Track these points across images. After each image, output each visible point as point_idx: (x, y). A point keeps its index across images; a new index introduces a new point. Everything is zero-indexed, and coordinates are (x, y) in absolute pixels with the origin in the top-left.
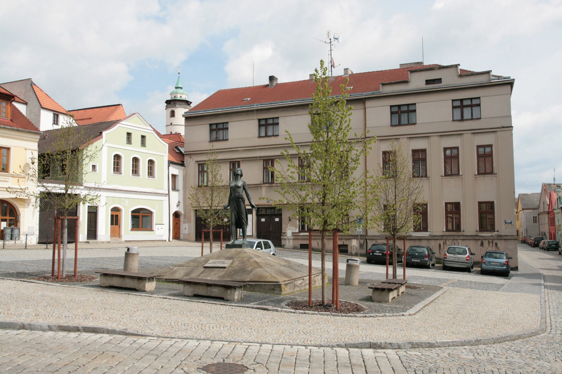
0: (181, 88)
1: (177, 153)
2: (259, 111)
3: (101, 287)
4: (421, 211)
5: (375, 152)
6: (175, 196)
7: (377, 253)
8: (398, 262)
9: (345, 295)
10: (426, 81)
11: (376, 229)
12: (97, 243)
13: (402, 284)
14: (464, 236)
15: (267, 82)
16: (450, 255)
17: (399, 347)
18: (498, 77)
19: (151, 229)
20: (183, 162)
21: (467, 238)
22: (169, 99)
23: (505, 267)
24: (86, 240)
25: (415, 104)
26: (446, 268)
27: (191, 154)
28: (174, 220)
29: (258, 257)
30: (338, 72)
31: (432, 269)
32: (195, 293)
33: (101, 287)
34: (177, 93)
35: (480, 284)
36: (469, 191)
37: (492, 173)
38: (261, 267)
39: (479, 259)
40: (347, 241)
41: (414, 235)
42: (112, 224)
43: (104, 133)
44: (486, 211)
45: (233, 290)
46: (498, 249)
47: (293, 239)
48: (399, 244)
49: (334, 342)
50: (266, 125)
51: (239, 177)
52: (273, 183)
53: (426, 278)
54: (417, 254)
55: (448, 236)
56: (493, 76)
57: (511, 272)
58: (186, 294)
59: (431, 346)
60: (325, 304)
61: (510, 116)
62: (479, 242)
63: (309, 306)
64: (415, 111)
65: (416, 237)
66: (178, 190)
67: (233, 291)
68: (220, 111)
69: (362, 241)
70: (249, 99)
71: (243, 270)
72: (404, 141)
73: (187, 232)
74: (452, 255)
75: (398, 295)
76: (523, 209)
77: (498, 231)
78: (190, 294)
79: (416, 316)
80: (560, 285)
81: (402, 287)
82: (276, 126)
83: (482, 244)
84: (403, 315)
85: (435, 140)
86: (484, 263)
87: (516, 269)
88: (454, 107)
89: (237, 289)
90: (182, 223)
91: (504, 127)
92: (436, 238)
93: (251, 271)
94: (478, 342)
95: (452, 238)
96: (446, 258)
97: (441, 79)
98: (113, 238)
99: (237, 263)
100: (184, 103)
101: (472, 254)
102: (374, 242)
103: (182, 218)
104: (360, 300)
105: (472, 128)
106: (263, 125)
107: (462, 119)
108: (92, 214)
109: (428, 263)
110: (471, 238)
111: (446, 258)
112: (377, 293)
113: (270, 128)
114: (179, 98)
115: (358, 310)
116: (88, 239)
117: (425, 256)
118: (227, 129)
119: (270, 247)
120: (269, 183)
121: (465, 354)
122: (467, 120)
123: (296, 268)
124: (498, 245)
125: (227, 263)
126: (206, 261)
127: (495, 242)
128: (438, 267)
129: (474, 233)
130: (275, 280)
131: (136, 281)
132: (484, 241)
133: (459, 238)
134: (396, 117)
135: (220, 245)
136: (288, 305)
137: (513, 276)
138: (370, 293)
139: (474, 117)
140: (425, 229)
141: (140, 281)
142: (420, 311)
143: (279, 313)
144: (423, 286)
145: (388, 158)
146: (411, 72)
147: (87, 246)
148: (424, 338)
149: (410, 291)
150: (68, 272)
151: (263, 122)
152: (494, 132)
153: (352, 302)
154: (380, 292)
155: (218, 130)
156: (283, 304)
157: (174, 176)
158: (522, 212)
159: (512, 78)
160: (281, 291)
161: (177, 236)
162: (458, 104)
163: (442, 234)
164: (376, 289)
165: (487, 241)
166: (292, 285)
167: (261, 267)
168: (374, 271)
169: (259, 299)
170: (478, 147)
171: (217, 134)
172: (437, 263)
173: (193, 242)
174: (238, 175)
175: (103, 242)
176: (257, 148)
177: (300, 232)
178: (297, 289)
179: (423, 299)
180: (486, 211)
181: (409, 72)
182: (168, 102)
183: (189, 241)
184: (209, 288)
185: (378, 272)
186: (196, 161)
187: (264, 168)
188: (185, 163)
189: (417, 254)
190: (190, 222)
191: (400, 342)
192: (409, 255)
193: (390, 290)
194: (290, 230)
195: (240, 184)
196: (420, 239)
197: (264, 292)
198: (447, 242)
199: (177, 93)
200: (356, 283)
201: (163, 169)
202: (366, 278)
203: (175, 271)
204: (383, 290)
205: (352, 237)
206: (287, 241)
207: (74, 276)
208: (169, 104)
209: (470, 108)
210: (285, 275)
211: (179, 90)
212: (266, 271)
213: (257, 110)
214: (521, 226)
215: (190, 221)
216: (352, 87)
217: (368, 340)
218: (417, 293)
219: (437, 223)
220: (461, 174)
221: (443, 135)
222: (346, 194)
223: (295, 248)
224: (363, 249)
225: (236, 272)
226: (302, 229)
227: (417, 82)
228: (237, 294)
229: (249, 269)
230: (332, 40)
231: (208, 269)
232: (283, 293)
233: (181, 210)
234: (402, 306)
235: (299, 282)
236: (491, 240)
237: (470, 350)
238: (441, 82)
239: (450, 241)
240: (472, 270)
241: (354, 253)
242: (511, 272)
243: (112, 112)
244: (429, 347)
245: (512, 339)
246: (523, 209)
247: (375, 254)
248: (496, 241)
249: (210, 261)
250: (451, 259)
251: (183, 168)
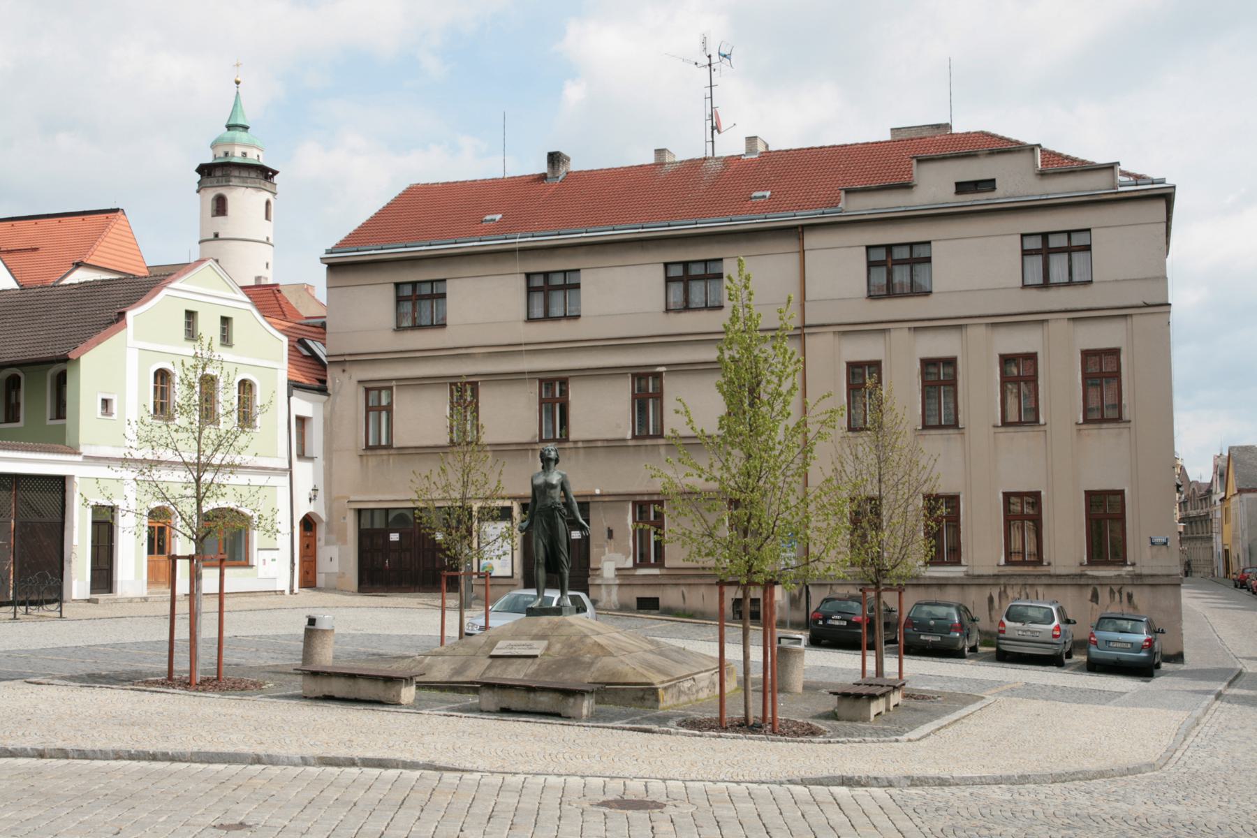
0: (246, 128)
1: (305, 357)
2: (526, 251)
4: (944, 516)
5: (828, 361)
6: (306, 475)
7: (836, 621)
8: (887, 643)
9: (786, 709)
10: (957, 184)
11: (833, 557)
12: (116, 601)
13: (895, 688)
14: (1050, 576)
15: (542, 167)
16: (1013, 624)
17: (890, 784)
18: (1137, 177)
19: (247, 565)
20: (324, 382)
21: (1057, 581)
22: (209, 159)
23: (1143, 654)
24: (88, 596)
25: (929, 243)
26: (1004, 657)
27: (344, 362)
28: (302, 537)
29: (598, 634)
30: (731, 145)
31: (970, 658)
32: (504, 705)
34: (232, 143)
35: (1073, 691)
36: (1064, 462)
37: (1119, 419)
38: (611, 655)
39: (1085, 636)
41: (927, 574)
42: (151, 552)
43: (131, 315)
44: (1105, 515)
45: (579, 698)
46: (1135, 608)
47: (620, 585)
48: (890, 599)
49: (783, 776)
50: (547, 289)
51: (552, 464)
52: (567, 440)
53: (950, 679)
54: (932, 622)
55: (1011, 576)
56: (1125, 174)
57: (1164, 665)
59: (942, 782)
60: (751, 722)
61: (1165, 278)
62: (1088, 593)
63: (721, 726)
64: (928, 260)
65: (931, 578)
66: (312, 459)
67: (579, 700)
68: (423, 249)
70: (498, 217)
71: (573, 661)
72: (900, 336)
73: (335, 567)
74: (1019, 625)
75: (888, 710)
76: (1240, 491)
77: (1133, 565)
78: (493, 708)
79: (921, 743)
80: (1252, 693)
81: (896, 693)
82: (573, 292)
83: (1095, 598)
84: (897, 741)
85: (977, 333)
86: (1095, 643)
87: (1178, 657)
88: (1025, 253)
89: (587, 696)
90: (320, 544)
91: (1148, 306)
92: (982, 581)
93: (592, 664)
94: (1024, 779)
95: (1020, 581)
96: (1003, 632)
97: (993, 180)
98: (154, 589)
99: (558, 646)
100: (253, 175)
101: (1068, 622)
102: (826, 593)
103: (321, 532)
104: (813, 717)
105: (1069, 307)
106: (538, 289)
107: (1046, 284)
108: (102, 527)
109: (960, 645)
110: (1068, 581)
111: (1003, 632)
112: (846, 702)
113: (557, 297)
114: (237, 158)
115: (813, 732)
116: (92, 593)
117: (953, 628)
118: (443, 296)
119: (585, 610)
120: (554, 440)
121: (998, 793)
122: (1058, 285)
123: (674, 655)
124: (1135, 598)
125: (538, 648)
126: (493, 645)
127: (1126, 590)
128: (986, 653)
129: (1075, 570)
130: (644, 680)
131: (380, 685)
132: (1099, 589)
133: (1037, 581)
134: (1036, 263)
135: (439, 602)
136: (679, 725)
137: (1166, 673)
138: (832, 703)
139: (1076, 278)
140: (955, 557)
141: (389, 684)
142: (929, 735)
143: (673, 737)
144: (940, 694)
145: (862, 376)
146: (920, 161)
147: (92, 610)
148: (932, 772)
149: (913, 703)
150: (204, 672)
151: (538, 282)
152: (1125, 316)
153: (800, 720)
154: (853, 700)
155: (419, 302)
156: (672, 723)
157: (301, 421)
158: (1237, 498)
159: (1169, 182)
160: (657, 700)
161: (310, 577)
162: (1035, 243)
163: (996, 571)
164: (844, 696)
165: (1108, 589)
166: (675, 690)
167: (611, 655)
168: (829, 664)
169: (626, 716)
170: (1086, 354)
171: (414, 310)
172: (984, 644)
173: (352, 593)
174: (550, 459)
175: (131, 600)
176: (523, 348)
177: (636, 566)
178: (684, 699)
179: (938, 717)
180: (1105, 515)
181: (914, 162)
182: (205, 171)
183: (343, 591)
184: (532, 695)
185: (843, 666)
186: (359, 382)
187: (542, 401)
188: (329, 384)
189: (932, 622)
190: (344, 542)
191: (892, 775)
192: (914, 625)
193: (872, 697)
194: (610, 562)
195: (555, 478)
196: (942, 584)
197: (629, 701)
198: (1009, 591)
199: (232, 143)
200: (799, 689)
201: (279, 406)
202: (814, 678)
203: (430, 667)
204: (858, 696)
206: (603, 590)
207: (218, 678)
208: (209, 175)
209: (1065, 256)
210: (660, 671)
211: (238, 134)
212: (622, 662)
213: (523, 250)
214: (1235, 538)
215: (342, 540)
216: (768, 194)
217: (838, 773)
218: (924, 705)
219: (984, 545)
220: (1042, 421)
221: (999, 322)
222: (789, 518)
223: (623, 608)
225: (561, 665)
226: (642, 561)
227: (935, 185)
228: (587, 706)
229: (588, 658)
230: (715, 58)
231: (500, 661)
232: (662, 705)
233: (318, 509)
234: (893, 726)
235: (686, 685)
236: (1116, 588)
237: (1009, 790)
238: (994, 189)
239: (1017, 589)
240: (1067, 661)
242: (1164, 665)
243: (99, 233)
244: (940, 785)
245: (1087, 776)
246: (1240, 491)
247: (830, 622)
248: (1129, 589)
249: (500, 644)
250: (1016, 635)
251: (324, 398)
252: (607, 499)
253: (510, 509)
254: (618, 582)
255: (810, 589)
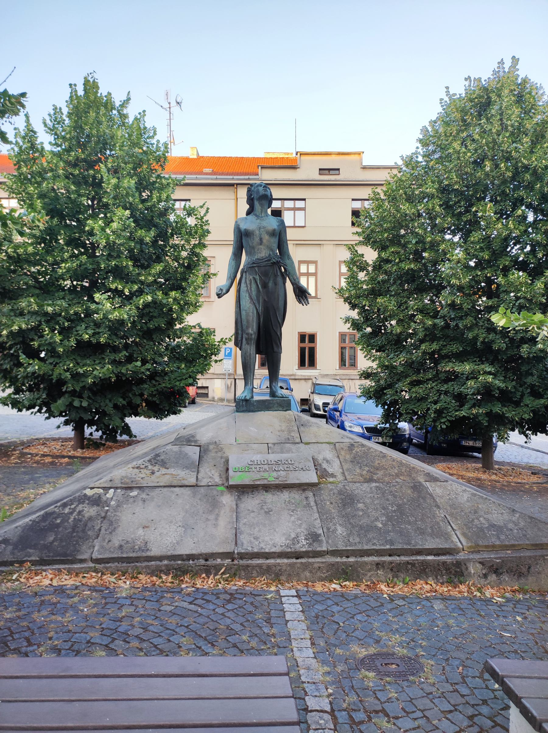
255: (237, 380)
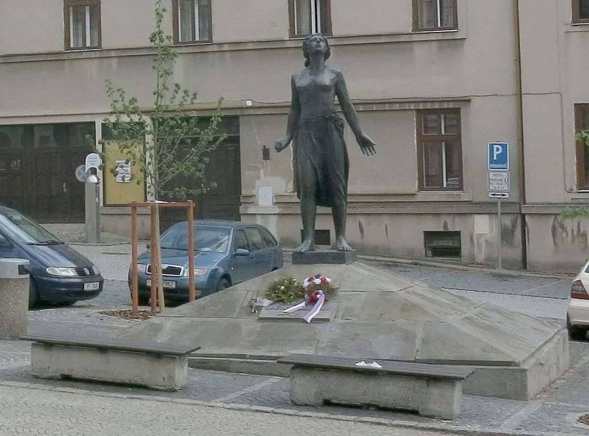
3: (36, 377)
33: (36, 378)
40: (458, 219)
58: (301, 397)
69: (507, 221)
163: (568, 198)
174: (318, 53)
195: (326, 79)
205: (475, 209)
224: (511, 244)
241: (481, 257)
252: (261, 112)
253: (141, 124)
254: (277, 211)
255: (527, 218)
